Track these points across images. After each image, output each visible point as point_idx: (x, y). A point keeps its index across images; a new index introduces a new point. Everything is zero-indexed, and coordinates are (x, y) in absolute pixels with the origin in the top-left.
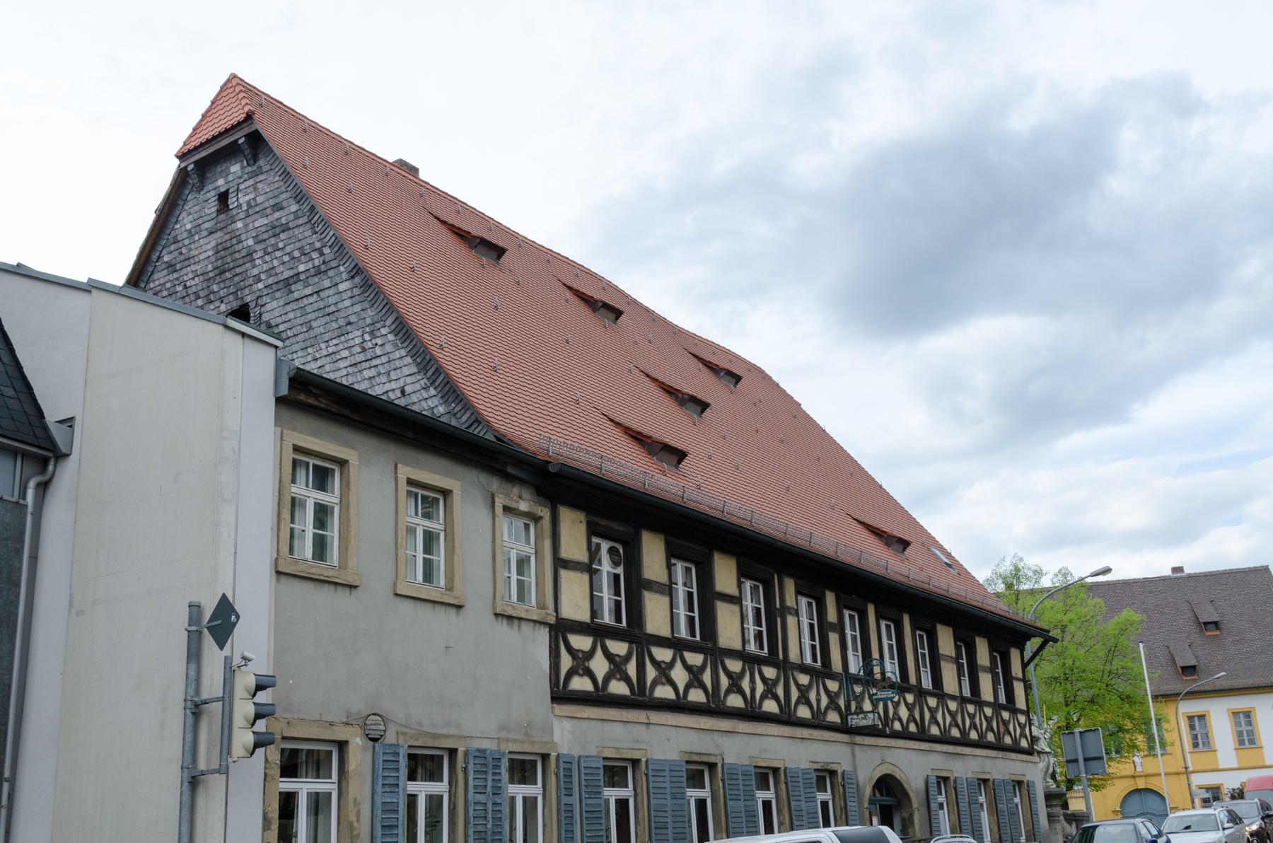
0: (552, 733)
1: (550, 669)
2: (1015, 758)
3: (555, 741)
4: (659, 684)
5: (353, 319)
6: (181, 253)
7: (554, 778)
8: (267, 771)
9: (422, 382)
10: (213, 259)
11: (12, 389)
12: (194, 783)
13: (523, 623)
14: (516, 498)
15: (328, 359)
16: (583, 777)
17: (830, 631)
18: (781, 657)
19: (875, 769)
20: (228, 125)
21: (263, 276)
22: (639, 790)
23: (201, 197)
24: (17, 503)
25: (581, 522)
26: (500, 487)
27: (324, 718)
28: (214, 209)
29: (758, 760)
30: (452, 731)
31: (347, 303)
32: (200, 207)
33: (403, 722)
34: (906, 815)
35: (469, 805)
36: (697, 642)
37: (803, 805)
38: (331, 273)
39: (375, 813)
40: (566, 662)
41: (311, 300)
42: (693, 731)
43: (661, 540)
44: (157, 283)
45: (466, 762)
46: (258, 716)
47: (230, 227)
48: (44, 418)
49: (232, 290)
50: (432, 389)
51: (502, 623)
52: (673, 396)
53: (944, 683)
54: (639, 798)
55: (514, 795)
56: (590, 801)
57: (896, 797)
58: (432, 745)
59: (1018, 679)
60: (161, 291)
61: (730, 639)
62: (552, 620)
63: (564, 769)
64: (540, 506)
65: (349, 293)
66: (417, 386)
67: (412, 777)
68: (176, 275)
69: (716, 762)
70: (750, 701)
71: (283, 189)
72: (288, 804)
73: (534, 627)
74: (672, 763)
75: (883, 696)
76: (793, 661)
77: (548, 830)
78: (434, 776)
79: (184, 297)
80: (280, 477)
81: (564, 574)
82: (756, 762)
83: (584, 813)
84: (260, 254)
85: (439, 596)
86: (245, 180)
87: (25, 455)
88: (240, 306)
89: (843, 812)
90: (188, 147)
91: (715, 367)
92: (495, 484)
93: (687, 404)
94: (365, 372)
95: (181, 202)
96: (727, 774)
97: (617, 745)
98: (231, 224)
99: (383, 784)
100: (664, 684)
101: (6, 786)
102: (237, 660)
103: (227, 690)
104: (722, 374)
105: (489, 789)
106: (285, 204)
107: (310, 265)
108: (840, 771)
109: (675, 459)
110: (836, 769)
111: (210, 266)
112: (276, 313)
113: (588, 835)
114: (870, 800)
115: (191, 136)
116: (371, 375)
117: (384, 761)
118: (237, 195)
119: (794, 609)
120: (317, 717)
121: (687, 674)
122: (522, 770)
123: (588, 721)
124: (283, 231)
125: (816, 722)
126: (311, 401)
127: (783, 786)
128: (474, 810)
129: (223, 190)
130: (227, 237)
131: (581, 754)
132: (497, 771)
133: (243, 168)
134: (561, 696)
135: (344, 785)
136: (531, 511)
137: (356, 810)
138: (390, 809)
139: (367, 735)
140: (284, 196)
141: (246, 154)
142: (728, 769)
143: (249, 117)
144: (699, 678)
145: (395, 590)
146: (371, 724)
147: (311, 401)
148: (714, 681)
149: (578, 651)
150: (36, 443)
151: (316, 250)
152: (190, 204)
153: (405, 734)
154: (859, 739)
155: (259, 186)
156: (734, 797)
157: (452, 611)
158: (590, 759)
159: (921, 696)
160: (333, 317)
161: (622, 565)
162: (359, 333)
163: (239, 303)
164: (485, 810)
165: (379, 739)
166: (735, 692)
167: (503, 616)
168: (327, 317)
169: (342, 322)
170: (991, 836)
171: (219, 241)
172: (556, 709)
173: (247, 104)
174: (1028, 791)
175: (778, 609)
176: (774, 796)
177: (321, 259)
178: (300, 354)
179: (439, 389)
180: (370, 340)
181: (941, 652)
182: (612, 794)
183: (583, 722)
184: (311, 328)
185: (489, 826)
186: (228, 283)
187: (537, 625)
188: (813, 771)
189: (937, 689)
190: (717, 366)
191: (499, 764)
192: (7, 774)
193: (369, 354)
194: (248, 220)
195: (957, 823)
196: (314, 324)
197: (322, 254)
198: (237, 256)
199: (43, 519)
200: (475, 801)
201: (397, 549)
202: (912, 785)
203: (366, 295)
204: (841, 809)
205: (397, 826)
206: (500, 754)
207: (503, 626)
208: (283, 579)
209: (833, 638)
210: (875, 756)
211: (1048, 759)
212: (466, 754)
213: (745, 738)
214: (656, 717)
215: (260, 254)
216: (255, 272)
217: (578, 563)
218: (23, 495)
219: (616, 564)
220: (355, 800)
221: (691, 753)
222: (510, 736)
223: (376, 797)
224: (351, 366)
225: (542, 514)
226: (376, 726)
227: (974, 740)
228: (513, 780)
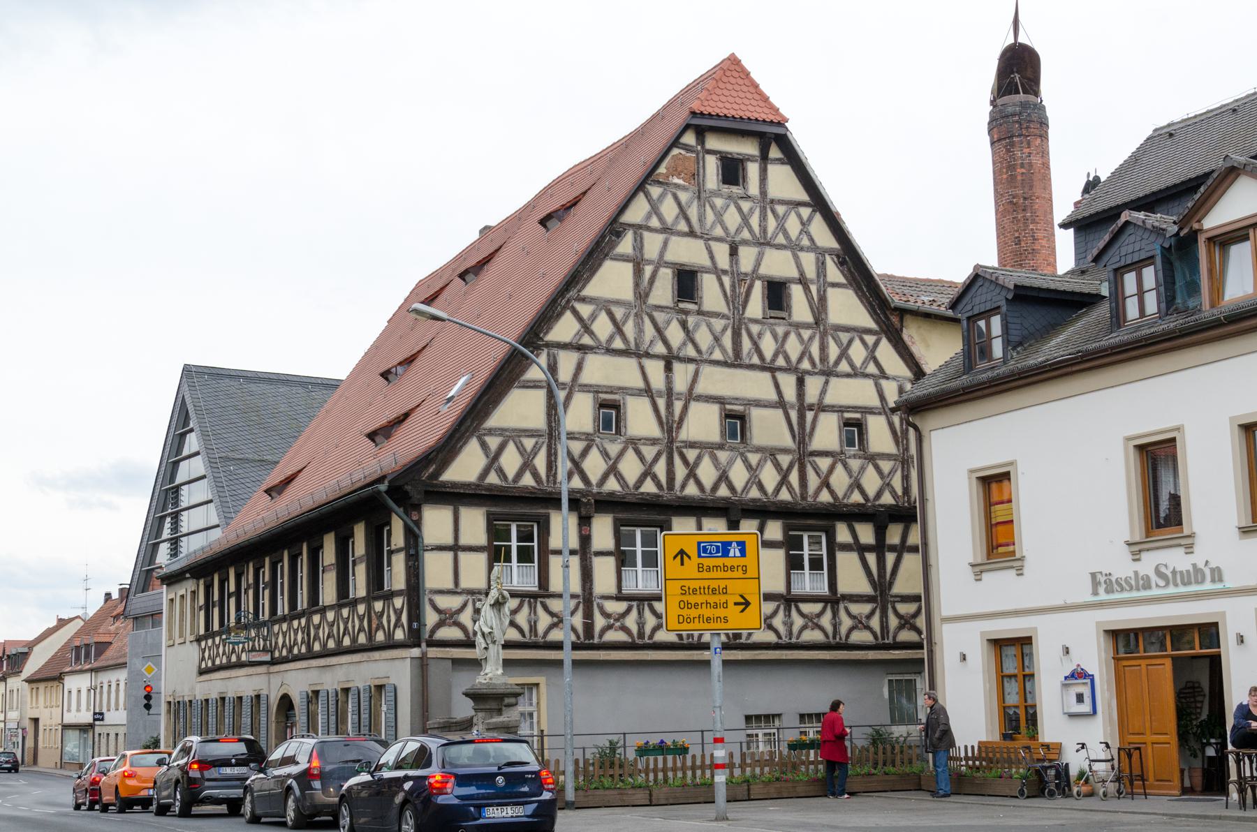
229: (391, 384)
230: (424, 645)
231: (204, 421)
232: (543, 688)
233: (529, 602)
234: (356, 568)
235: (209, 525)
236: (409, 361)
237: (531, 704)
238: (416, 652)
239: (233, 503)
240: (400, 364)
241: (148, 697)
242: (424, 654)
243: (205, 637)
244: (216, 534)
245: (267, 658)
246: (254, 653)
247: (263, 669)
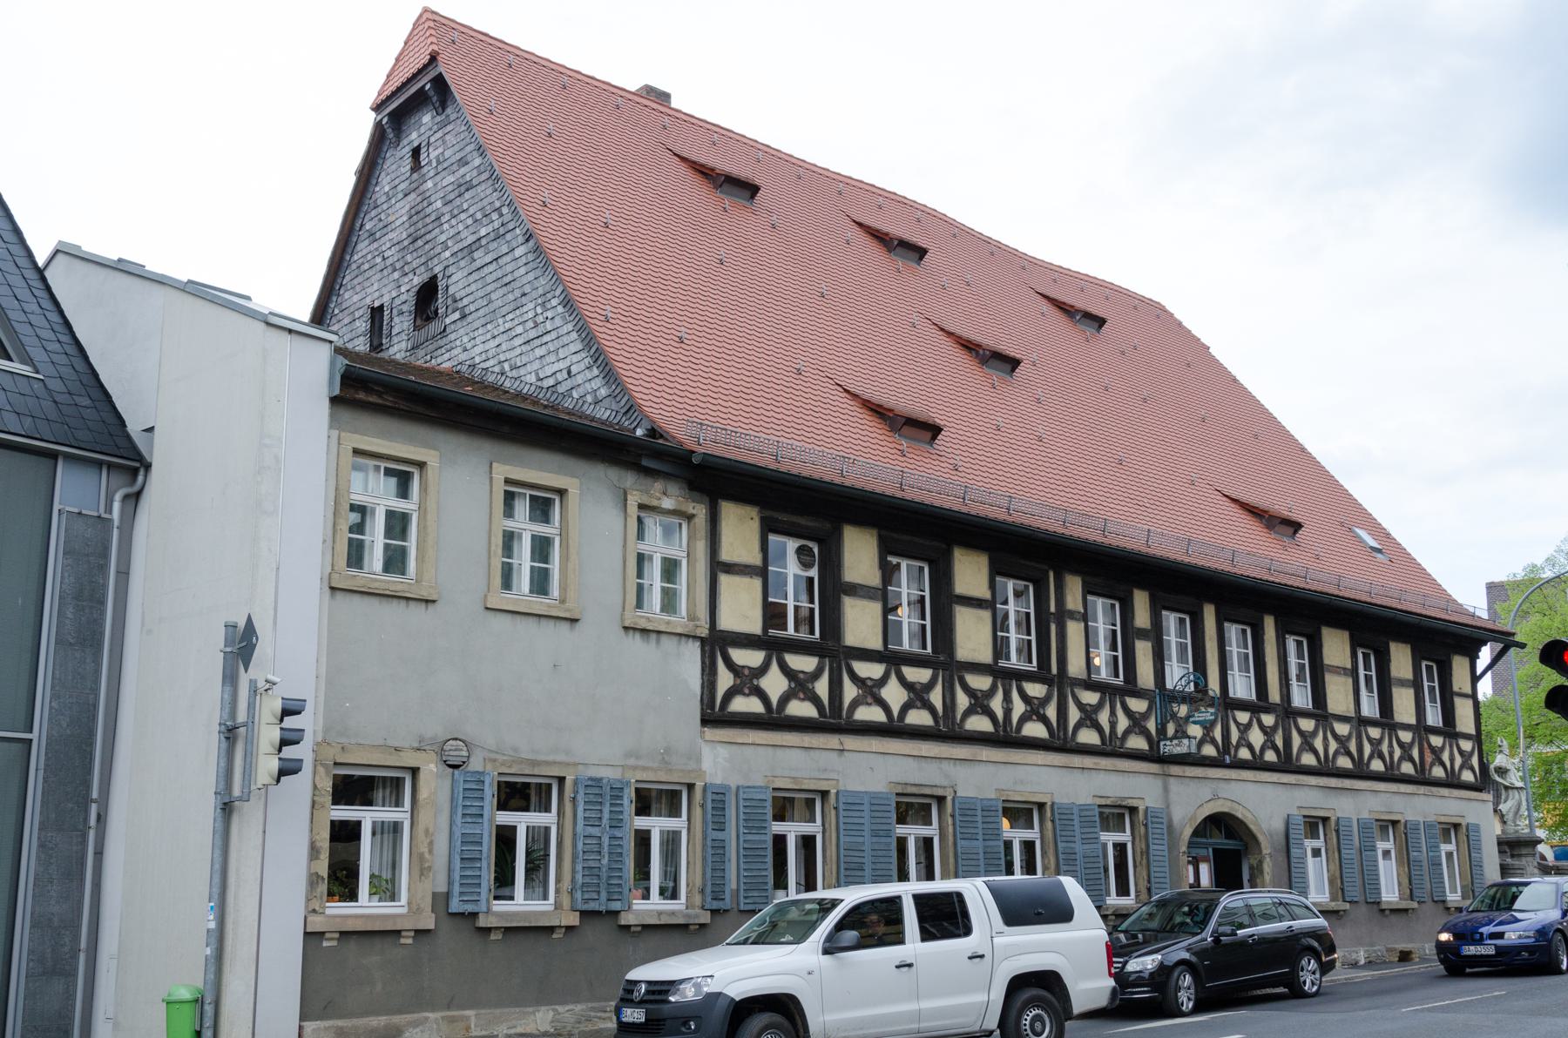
0: (699, 760)
1: (703, 687)
2: (1447, 795)
3: (704, 769)
4: (862, 704)
5: (527, 289)
6: (380, 220)
7: (950, 821)
8: (316, 798)
9: (586, 361)
10: (407, 225)
11: (88, 398)
12: (227, 809)
13: (664, 638)
14: (657, 494)
15: (505, 337)
16: (742, 809)
17: (1139, 639)
18: (1054, 670)
19: (1201, 805)
20: (414, 70)
21: (450, 243)
22: (827, 826)
23: (399, 154)
24: (99, 517)
25: (752, 519)
26: (636, 483)
27: (390, 742)
28: (408, 167)
29: (1010, 793)
30: (561, 758)
31: (522, 271)
32: (397, 163)
33: (494, 748)
34: (1254, 862)
35: (578, 838)
36: (928, 655)
37: (1078, 847)
38: (508, 237)
39: (453, 845)
40: (725, 680)
41: (491, 268)
42: (910, 759)
43: (872, 536)
44: (360, 254)
45: (575, 792)
46: (284, 742)
47: (421, 188)
48: (125, 426)
49: (423, 260)
50: (595, 368)
51: (634, 636)
52: (973, 352)
53: (1329, 701)
54: (827, 834)
55: (547, 825)
56: (750, 837)
57: (1241, 840)
58: (531, 773)
60: (363, 264)
61: (974, 650)
62: (704, 632)
63: (713, 800)
64: (693, 501)
65: (524, 260)
66: (582, 366)
67: (901, 820)
68: (375, 245)
69: (945, 795)
71: (468, 140)
72: (345, 834)
73: (680, 641)
74: (874, 796)
75: (1201, 719)
76: (1073, 676)
77: (691, 866)
78: (674, 812)
79: (382, 270)
80: (337, 484)
81: (724, 579)
82: (1008, 795)
83: (742, 850)
84: (447, 217)
85: (546, 609)
86: (435, 132)
87: (110, 466)
88: (430, 278)
89: (1144, 857)
90: (381, 97)
91: (1070, 309)
92: (629, 479)
93: (989, 362)
94: (537, 350)
95: (380, 161)
96: (960, 809)
97: (793, 774)
98: (422, 184)
99: (463, 814)
100: (869, 704)
101: (94, 808)
102: (261, 684)
103: (251, 715)
104: (1078, 318)
105: (605, 821)
106: (469, 158)
107: (490, 228)
108: (1141, 808)
109: (929, 435)
110: (1135, 805)
111: (405, 233)
112: (460, 285)
113: (745, 874)
114: (1190, 843)
115: (385, 84)
116: (542, 354)
117: (464, 789)
118: (428, 150)
119: (1079, 613)
120: (381, 742)
121: (906, 693)
122: (783, 808)
123: (752, 747)
124: (467, 190)
125: (1109, 748)
126: (373, 399)
127: (1049, 825)
128: (584, 844)
129: (416, 144)
130: (419, 199)
131: (740, 784)
132: (618, 802)
133: (433, 118)
134: (715, 716)
135: (415, 812)
136: (678, 508)
137: (428, 841)
138: (472, 840)
139: (445, 761)
140: (469, 148)
141: (434, 101)
142: (960, 803)
143: (433, 59)
144: (923, 698)
145: (485, 604)
146: (450, 750)
147: (373, 399)
148: (948, 701)
149: (743, 667)
150: (119, 454)
151: (496, 210)
152: (388, 163)
153: (495, 760)
154: (1175, 769)
155: (447, 137)
156: (966, 836)
157: (565, 626)
158: (753, 790)
159: (1288, 717)
160: (509, 288)
161: (816, 567)
162: (531, 305)
163: (429, 275)
164: (600, 844)
165: (460, 766)
166: (979, 714)
167: (634, 629)
168: (505, 288)
169: (517, 293)
170: (1399, 891)
171: (413, 204)
172: (707, 733)
173: (432, 43)
174: (1468, 836)
175: (1052, 614)
176: (1038, 835)
177: (500, 220)
178: (480, 331)
179: (601, 368)
180: (542, 313)
181: (1327, 661)
182: (1110, 838)
183: (744, 747)
184: (490, 302)
185: (605, 861)
186: (420, 252)
187: (683, 639)
188: (1096, 807)
189: (1318, 709)
190: (1072, 307)
191: (621, 794)
192: (95, 795)
193: (541, 330)
194: (438, 178)
195: (1338, 874)
196: (493, 296)
197: (501, 215)
198: (428, 220)
199: (134, 532)
200: (586, 834)
201: (489, 558)
202: (1263, 826)
203: (538, 261)
204: (1141, 852)
205: (481, 859)
206: (622, 783)
207: (636, 640)
208: (339, 595)
209: (1143, 650)
210: (1205, 791)
211: (1520, 796)
212: (576, 782)
213: (991, 768)
214: (851, 742)
215: (447, 217)
216: (443, 238)
217: (746, 566)
218: (109, 509)
219: (806, 565)
220: (427, 831)
221: (906, 784)
222: (640, 763)
223: (454, 827)
224: (525, 343)
225: (694, 512)
226: (457, 752)
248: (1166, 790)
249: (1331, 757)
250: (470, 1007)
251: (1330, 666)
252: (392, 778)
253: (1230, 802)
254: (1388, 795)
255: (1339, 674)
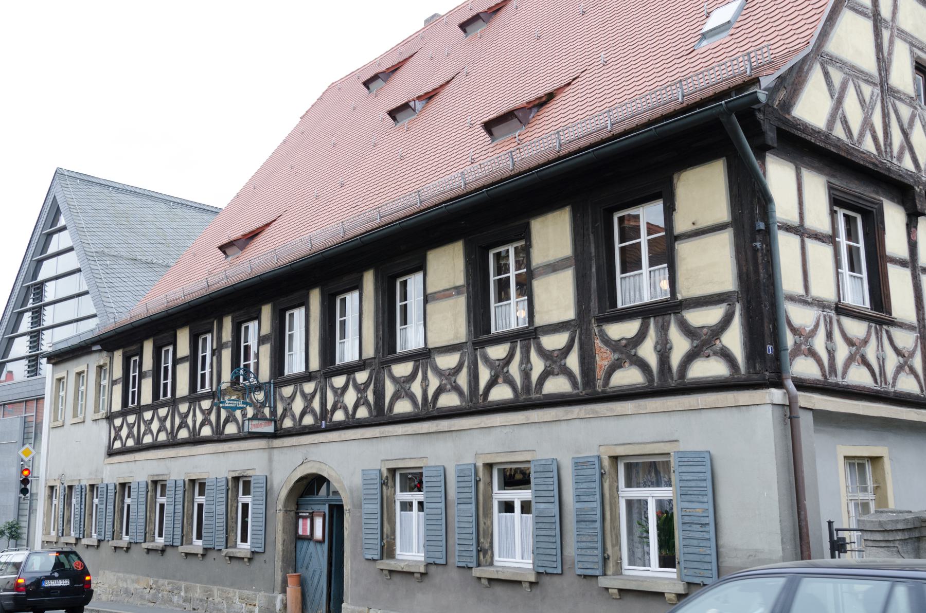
59: (788, 228)
70: (194, 432)
75: (233, 405)
157: (82, 424)
202: (345, 483)
210: (296, 457)
213: (184, 460)
227: (131, 447)
228: (631, 483)
229: (399, 125)
230: (790, 384)
231: (78, 218)
232: (887, 464)
233: (876, 328)
234: (143, 381)
235: (80, 316)
236: (429, 97)
237: (865, 490)
238: (776, 395)
239: (111, 294)
240: (419, 98)
241: (25, 481)
242: (792, 401)
243: (124, 413)
244: (91, 324)
245: (270, 429)
246: (255, 422)
247: (261, 443)
248: (270, 460)
249: (430, 398)
250: (199, 583)
251: (435, 293)
252: (663, 462)
253: (319, 463)
254: (507, 430)
255: (450, 296)
